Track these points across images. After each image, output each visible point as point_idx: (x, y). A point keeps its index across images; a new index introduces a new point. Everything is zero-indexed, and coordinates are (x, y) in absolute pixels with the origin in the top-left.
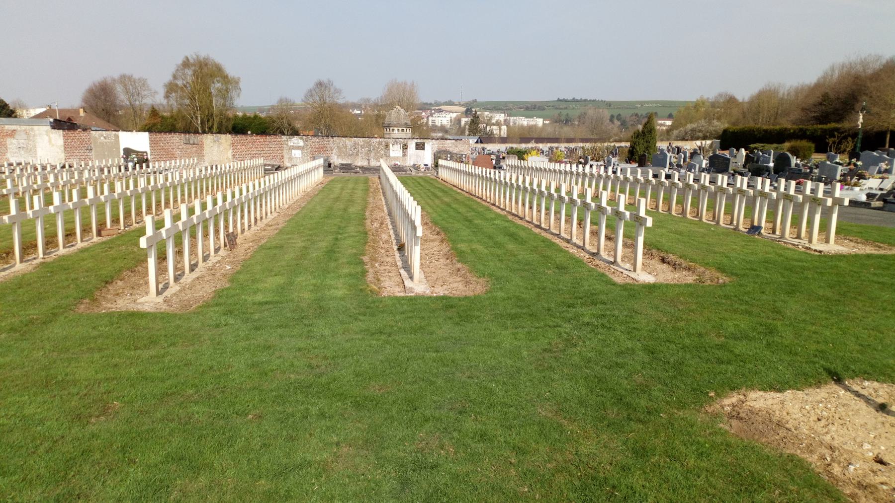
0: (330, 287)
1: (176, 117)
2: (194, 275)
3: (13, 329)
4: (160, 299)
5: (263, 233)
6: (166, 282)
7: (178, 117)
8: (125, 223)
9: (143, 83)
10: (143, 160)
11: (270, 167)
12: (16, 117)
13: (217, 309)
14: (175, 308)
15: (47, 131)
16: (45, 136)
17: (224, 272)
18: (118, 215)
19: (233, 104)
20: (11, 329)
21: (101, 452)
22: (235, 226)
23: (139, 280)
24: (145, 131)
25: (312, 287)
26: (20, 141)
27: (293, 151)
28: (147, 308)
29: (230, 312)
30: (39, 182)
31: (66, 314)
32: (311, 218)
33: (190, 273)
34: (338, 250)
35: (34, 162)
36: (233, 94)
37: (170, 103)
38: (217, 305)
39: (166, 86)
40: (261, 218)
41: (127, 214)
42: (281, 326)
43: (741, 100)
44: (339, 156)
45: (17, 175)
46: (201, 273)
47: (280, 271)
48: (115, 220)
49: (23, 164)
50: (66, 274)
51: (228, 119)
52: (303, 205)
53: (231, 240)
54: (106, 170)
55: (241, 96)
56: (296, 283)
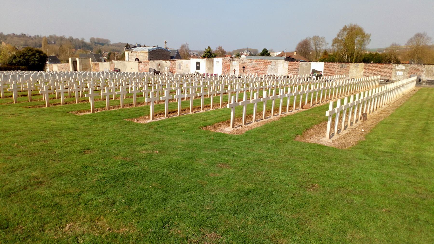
0: (425, 150)
1: (335, 55)
2: (346, 132)
3: (273, 143)
4: (330, 141)
5: (380, 115)
6: (333, 133)
7: (337, 55)
8: (312, 103)
9: (323, 39)
10: (319, 75)
11: (383, 80)
12: (270, 56)
13: (360, 150)
14: (337, 146)
15: (283, 62)
17: (361, 132)
18: (310, 99)
19: (365, 48)
20: (272, 143)
21: (314, 205)
22: (366, 110)
23: (320, 130)
25: (413, 148)
26: (273, 66)
27: (398, 72)
28: (324, 144)
29: (367, 154)
30: (275, 84)
31: (292, 140)
32: (410, 109)
33: (344, 130)
34: (429, 129)
35: (277, 75)
36: (366, 42)
37: (334, 48)
38: (359, 148)
39: (333, 40)
40: (379, 107)
41: (314, 100)
42: (396, 166)
44: (426, 75)
45: (267, 80)
46: (349, 131)
47: (393, 137)
48: (309, 102)
49: (270, 76)
51: (361, 56)
52: (404, 102)
53: (364, 117)
54: (298, 80)
55: (370, 43)
56: (403, 144)
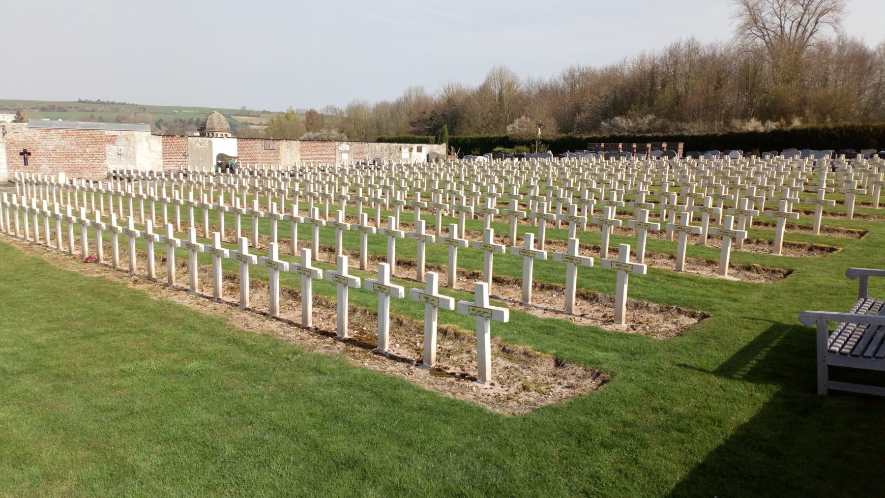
15: (147, 138)
16: (145, 142)
43: (319, 113)
50: (711, 292)
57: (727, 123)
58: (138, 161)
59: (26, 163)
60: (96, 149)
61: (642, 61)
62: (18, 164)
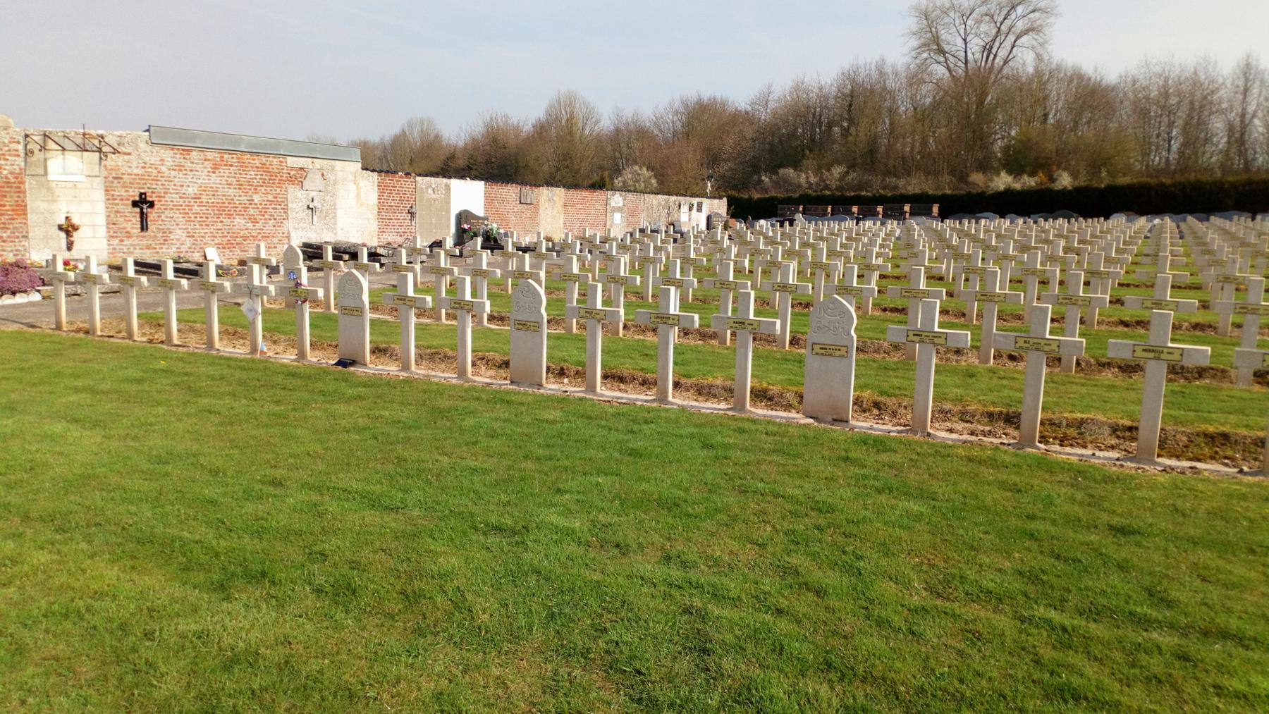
15: (355, 174)
24: (474, 178)
57: (963, 178)
58: (340, 225)
59: (144, 227)
60: (270, 197)
61: (1148, 65)
62: (129, 225)
